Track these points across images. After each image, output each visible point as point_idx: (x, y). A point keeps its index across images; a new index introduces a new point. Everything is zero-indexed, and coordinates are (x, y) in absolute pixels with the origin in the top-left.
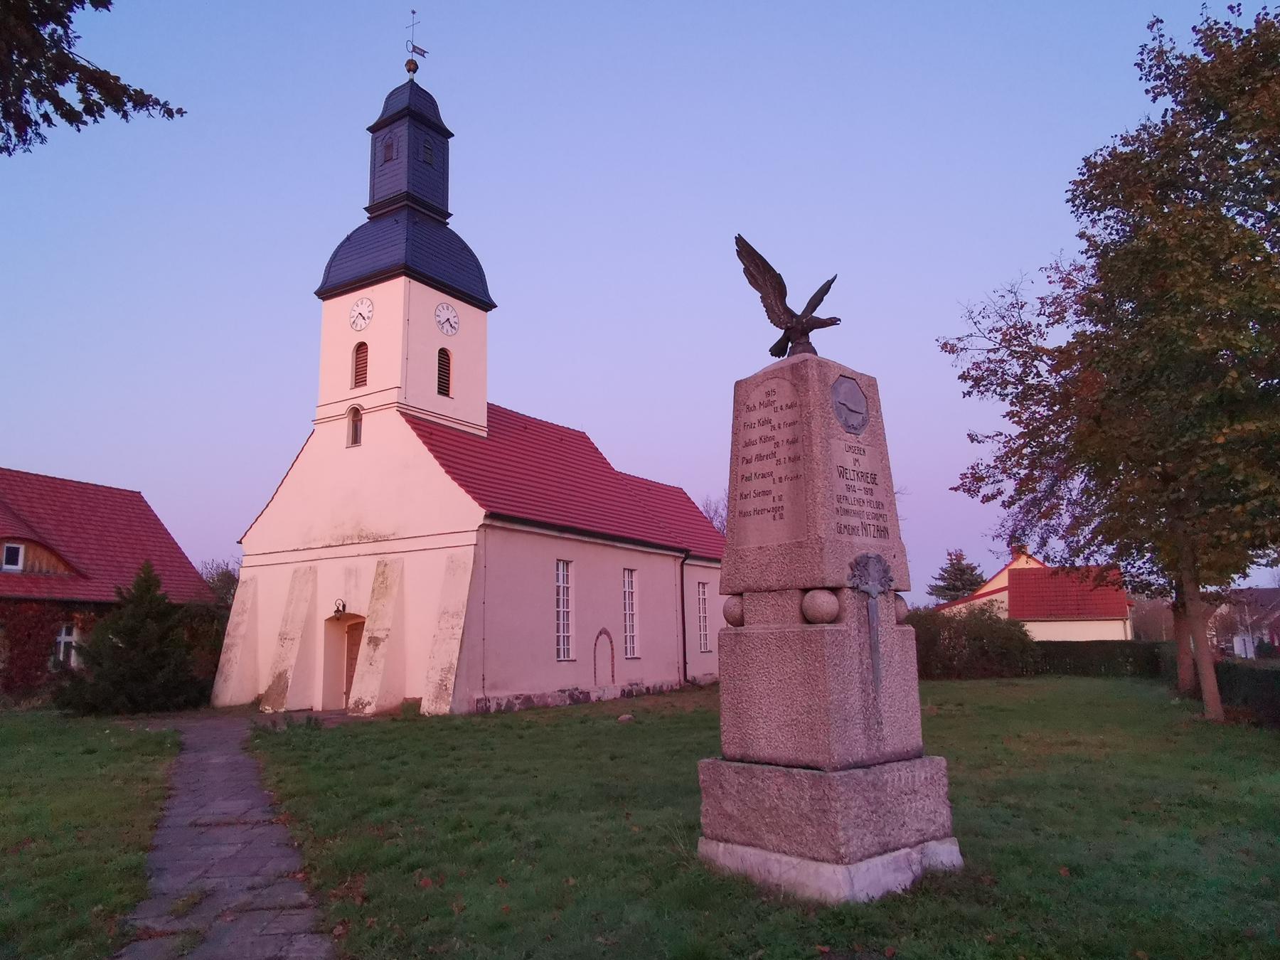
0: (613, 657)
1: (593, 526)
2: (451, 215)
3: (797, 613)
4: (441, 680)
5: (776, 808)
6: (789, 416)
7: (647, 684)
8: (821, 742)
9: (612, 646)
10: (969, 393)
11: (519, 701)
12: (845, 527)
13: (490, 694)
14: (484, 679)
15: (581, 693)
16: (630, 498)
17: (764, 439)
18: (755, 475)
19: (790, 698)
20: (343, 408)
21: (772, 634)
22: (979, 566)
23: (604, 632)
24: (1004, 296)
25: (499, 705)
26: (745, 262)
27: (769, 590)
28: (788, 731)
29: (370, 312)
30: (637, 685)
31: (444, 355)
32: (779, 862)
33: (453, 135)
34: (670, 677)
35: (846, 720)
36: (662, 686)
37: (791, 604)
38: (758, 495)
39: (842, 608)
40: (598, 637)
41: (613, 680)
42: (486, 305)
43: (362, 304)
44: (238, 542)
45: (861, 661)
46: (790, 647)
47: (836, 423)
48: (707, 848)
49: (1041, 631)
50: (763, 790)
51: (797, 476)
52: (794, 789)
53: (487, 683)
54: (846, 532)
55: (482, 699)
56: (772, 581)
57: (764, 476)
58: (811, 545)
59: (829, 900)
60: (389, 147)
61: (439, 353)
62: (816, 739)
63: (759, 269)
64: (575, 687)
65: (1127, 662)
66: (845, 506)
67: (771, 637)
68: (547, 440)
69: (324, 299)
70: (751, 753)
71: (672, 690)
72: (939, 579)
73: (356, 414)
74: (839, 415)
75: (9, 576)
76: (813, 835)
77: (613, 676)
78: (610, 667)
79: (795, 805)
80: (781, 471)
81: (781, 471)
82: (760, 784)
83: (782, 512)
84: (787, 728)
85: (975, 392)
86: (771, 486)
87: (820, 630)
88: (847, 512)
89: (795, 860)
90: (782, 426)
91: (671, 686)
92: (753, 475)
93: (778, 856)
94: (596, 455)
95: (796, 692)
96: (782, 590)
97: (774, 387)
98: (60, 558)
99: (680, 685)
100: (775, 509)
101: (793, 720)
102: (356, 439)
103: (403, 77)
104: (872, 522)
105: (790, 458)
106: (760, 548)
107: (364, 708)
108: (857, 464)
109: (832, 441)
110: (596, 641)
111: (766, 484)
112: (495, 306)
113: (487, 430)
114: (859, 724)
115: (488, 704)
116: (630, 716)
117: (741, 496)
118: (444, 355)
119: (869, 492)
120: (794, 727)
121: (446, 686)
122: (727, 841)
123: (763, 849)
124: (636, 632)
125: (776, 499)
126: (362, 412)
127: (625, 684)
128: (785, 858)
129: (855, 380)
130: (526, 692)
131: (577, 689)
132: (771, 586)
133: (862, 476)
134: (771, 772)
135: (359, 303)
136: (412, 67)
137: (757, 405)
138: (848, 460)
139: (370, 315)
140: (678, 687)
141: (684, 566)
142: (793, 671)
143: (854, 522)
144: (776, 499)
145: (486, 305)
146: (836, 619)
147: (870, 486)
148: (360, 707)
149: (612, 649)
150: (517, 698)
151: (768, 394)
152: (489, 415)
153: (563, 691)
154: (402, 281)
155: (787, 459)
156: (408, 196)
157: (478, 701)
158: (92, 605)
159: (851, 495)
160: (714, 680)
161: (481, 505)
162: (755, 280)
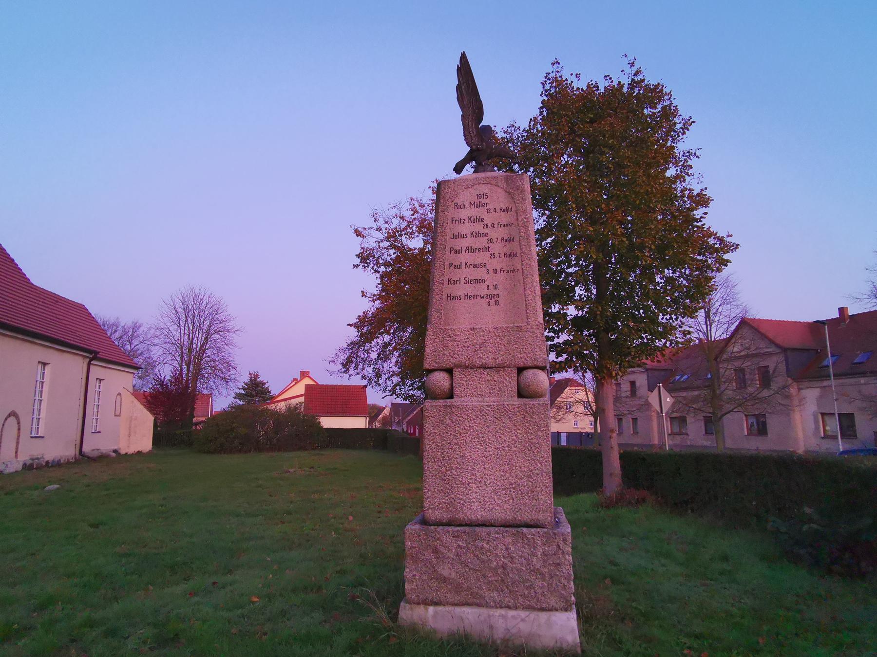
1: (4, 319)
3: (515, 389)
5: (504, 567)
7: (46, 459)
8: (542, 502)
10: (358, 266)
19: (508, 464)
21: (490, 406)
22: (267, 382)
23: (13, 414)
26: (461, 79)
27: (484, 367)
28: (505, 494)
30: (38, 459)
32: (504, 617)
34: (68, 452)
36: (60, 460)
37: (510, 381)
41: (16, 456)
46: (510, 418)
48: (408, 613)
49: (328, 422)
50: (489, 550)
52: (523, 547)
56: (488, 358)
58: (531, 330)
59: (564, 646)
62: (536, 500)
63: (468, 90)
65: (371, 440)
67: (488, 408)
70: (460, 516)
71: (68, 463)
72: (242, 389)
76: (542, 587)
77: (16, 452)
78: (15, 445)
79: (525, 562)
82: (485, 545)
83: (498, 299)
84: (504, 492)
85: (361, 266)
87: (543, 404)
89: (523, 614)
91: (68, 459)
92: (463, 264)
93: (503, 612)
95: (515, 458)
96: (499, 368)
97: (486, 191)
99: (75, 458)
100: (488, 296)
101: (512, 484)
105: (505, 254)
106: (473, 329)
110: (4, 422)
116: (58, 486)
120: (512, 489)
122: (436, 604)
123: (481, 606)
124: (43, 415)
125: (491, 287)
127: (27, 458)
128: (512, 613)
132: (486, 364)
134: (498, 533)
137: (467, 204)
140: (73, 461)
142: (513, 440)
144: (491, 287)
149: (19, 429)
155: (502, 254)
160: (100, 454)
162: (462, 99)
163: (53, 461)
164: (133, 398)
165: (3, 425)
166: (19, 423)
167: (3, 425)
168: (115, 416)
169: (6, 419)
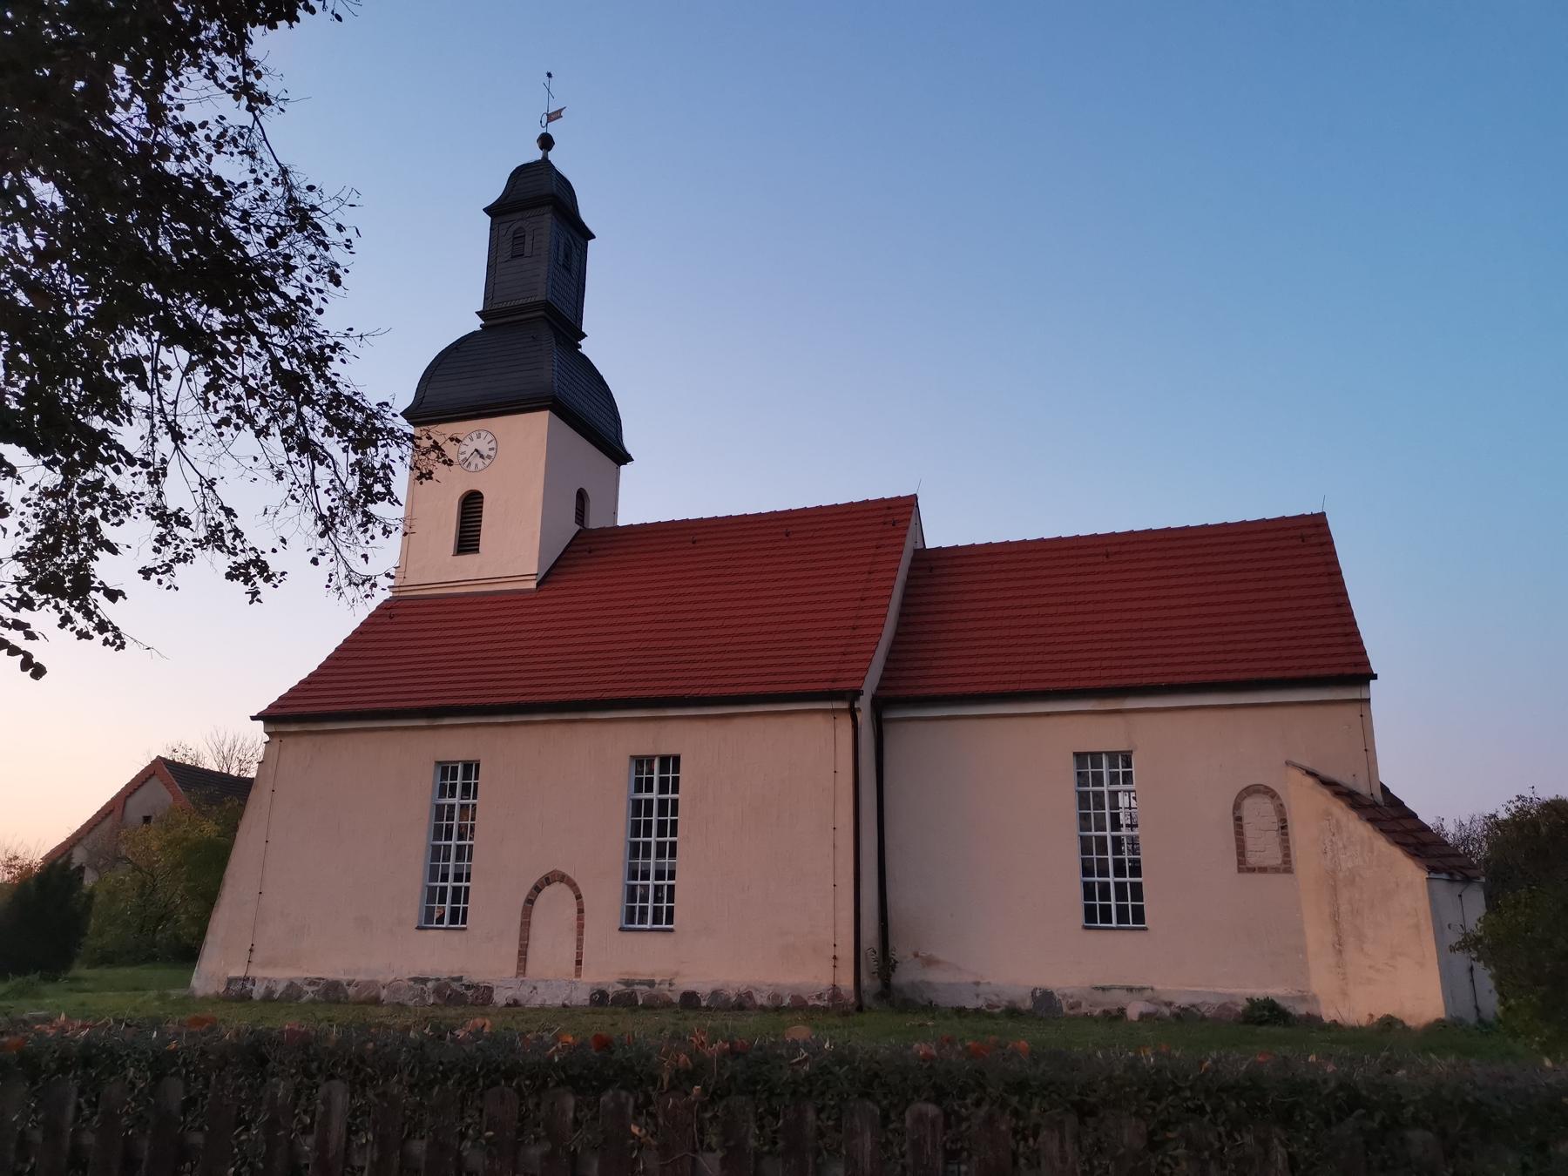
2: (584, 336)
13: (256, 972)
15: (468, 987)
24: (458, 441)
29: (491, 449)
30: (651, 984)
33: (593, 237)
42: (476, 313)
43: (479, 437)
53: (256, 957)
55: (236, 979)
60: (518, 238)
68: (750, 647)
103: (537, 155)
115: (249, 986)
130: (330, 976)
131: (460, 979)
135: (474, 436)
136: (546, 142)
139: (492, 453)
145: (476, 313)
149: (581, 911)
150: (312, 982)
153: (424, 981)
154: (548, 412)
156: (547, 306)
157: (231, 981)
158: (210, 829)
163: (715, 994)
165: (530, 901)
166: (579, 897)
167: (530, 901)
169: (537, 889)
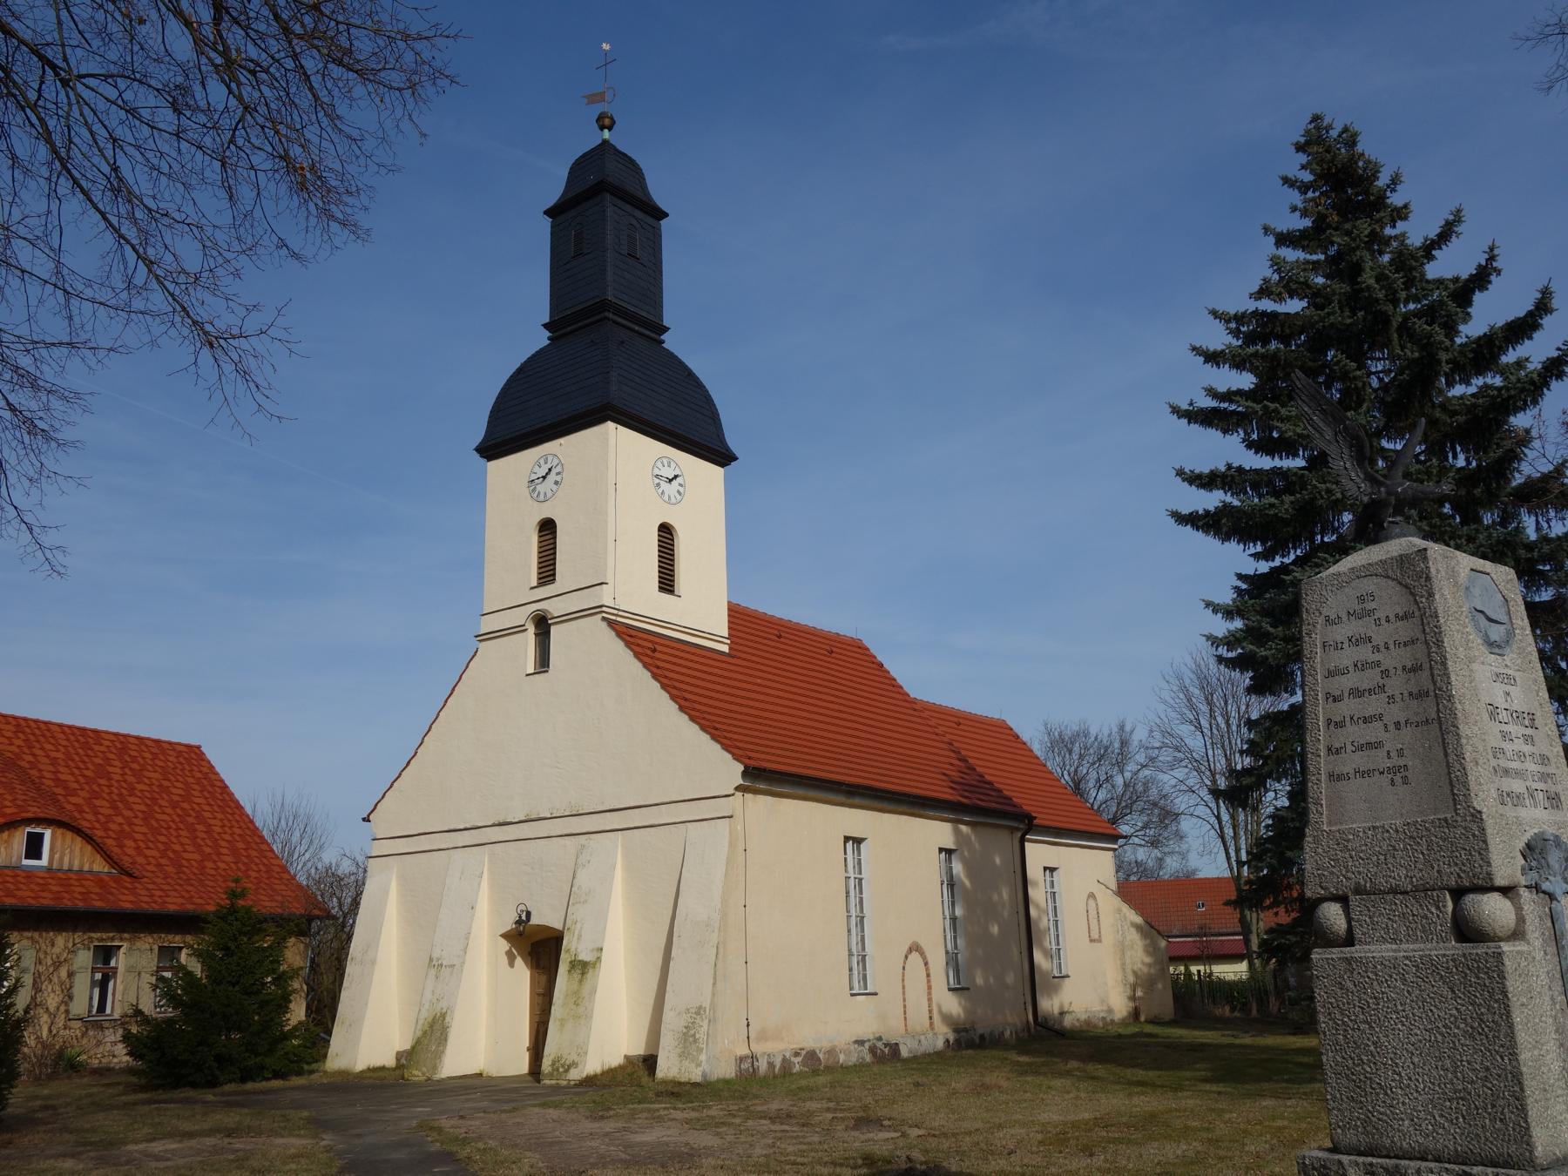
0: (929, 988)
4: (686, 1027)
6: (1405, 630)
7: (980, 1031)
9: (927, 969)
11: (799, 1059)
12: (1508, 795)
13: (757, 1048)
14: (748, 1025)
15: (886, 1045)
16: (937, 738)
17: (1361, 666)
18: (1352, 718)
20: (521, 616)
23: (915, 948)
25: (771, 1065)
31: (666, 531)
33: (666, 215)
35: (1545, 1090)
38: (1361, 748)
39: (1521, 920)
40: (906, 957)
43: (679, 492)
44: (364, 819)
45: (1552, 999)
47: (1475, 637)
51: (1427, 720)
54: (1510, 804)
55: (746, 1057)
56: (1400, 877)
57: (1366, 720)
58: (1463, 824)
61: (659, 530)
64: (877, 1035)
66: (1503, 763)
69: (490, 458)
73: (543, 624)
74: (1477, 627)
75: (30, 874)
80: (1396, 713)
81: (1396, 713)
83: (1407, 773)
86: (1381, 735)
88: (1506, 772)
90: (1392, 647)
92: (1348, 719)
94: (881, 674)
97: (1372, 588)
98: (99, 848)
100: (1394, 770)
102: (543, 662)
103: (594, 138)
104: (1540, 786)
107: (567, 1071)
108: (1509, 699)
109: (1475, 666)
110: (905, 963)
111: (1374, 732)
112: (735, 459)
113: (729, 642)
114: (1562, 1096)
117: (1329, 750)
118: (666, 531)
119: (1529, 739)
121: (694, 1035)
126: (550, 622)
129: (1488, 574)
130: (809, 1044)
131: (880, 1039)
133: (1517, 716)
135: (681, 489)
138: (1497, 693)
141: (1026, 844)
143: (1517, 786)
146: (1517, 934)
147: (1529, 731)
148: (561, 1070)
150: (797, 1054)
151: (1361, 599)
152: (733, 620)
153: (860, 1042)
157: (742, 1059)
159: (1508, 746)
161: (737, 758)
163: (991, 1034)
164: (1117, 901)
168: (1091, 941)
